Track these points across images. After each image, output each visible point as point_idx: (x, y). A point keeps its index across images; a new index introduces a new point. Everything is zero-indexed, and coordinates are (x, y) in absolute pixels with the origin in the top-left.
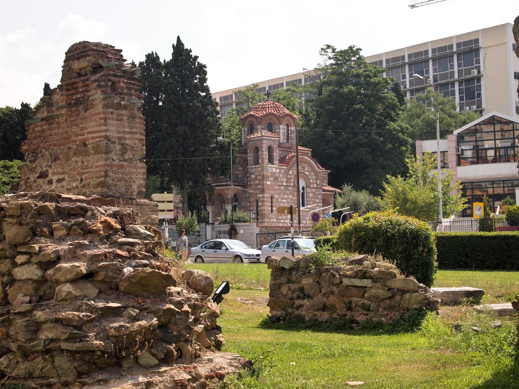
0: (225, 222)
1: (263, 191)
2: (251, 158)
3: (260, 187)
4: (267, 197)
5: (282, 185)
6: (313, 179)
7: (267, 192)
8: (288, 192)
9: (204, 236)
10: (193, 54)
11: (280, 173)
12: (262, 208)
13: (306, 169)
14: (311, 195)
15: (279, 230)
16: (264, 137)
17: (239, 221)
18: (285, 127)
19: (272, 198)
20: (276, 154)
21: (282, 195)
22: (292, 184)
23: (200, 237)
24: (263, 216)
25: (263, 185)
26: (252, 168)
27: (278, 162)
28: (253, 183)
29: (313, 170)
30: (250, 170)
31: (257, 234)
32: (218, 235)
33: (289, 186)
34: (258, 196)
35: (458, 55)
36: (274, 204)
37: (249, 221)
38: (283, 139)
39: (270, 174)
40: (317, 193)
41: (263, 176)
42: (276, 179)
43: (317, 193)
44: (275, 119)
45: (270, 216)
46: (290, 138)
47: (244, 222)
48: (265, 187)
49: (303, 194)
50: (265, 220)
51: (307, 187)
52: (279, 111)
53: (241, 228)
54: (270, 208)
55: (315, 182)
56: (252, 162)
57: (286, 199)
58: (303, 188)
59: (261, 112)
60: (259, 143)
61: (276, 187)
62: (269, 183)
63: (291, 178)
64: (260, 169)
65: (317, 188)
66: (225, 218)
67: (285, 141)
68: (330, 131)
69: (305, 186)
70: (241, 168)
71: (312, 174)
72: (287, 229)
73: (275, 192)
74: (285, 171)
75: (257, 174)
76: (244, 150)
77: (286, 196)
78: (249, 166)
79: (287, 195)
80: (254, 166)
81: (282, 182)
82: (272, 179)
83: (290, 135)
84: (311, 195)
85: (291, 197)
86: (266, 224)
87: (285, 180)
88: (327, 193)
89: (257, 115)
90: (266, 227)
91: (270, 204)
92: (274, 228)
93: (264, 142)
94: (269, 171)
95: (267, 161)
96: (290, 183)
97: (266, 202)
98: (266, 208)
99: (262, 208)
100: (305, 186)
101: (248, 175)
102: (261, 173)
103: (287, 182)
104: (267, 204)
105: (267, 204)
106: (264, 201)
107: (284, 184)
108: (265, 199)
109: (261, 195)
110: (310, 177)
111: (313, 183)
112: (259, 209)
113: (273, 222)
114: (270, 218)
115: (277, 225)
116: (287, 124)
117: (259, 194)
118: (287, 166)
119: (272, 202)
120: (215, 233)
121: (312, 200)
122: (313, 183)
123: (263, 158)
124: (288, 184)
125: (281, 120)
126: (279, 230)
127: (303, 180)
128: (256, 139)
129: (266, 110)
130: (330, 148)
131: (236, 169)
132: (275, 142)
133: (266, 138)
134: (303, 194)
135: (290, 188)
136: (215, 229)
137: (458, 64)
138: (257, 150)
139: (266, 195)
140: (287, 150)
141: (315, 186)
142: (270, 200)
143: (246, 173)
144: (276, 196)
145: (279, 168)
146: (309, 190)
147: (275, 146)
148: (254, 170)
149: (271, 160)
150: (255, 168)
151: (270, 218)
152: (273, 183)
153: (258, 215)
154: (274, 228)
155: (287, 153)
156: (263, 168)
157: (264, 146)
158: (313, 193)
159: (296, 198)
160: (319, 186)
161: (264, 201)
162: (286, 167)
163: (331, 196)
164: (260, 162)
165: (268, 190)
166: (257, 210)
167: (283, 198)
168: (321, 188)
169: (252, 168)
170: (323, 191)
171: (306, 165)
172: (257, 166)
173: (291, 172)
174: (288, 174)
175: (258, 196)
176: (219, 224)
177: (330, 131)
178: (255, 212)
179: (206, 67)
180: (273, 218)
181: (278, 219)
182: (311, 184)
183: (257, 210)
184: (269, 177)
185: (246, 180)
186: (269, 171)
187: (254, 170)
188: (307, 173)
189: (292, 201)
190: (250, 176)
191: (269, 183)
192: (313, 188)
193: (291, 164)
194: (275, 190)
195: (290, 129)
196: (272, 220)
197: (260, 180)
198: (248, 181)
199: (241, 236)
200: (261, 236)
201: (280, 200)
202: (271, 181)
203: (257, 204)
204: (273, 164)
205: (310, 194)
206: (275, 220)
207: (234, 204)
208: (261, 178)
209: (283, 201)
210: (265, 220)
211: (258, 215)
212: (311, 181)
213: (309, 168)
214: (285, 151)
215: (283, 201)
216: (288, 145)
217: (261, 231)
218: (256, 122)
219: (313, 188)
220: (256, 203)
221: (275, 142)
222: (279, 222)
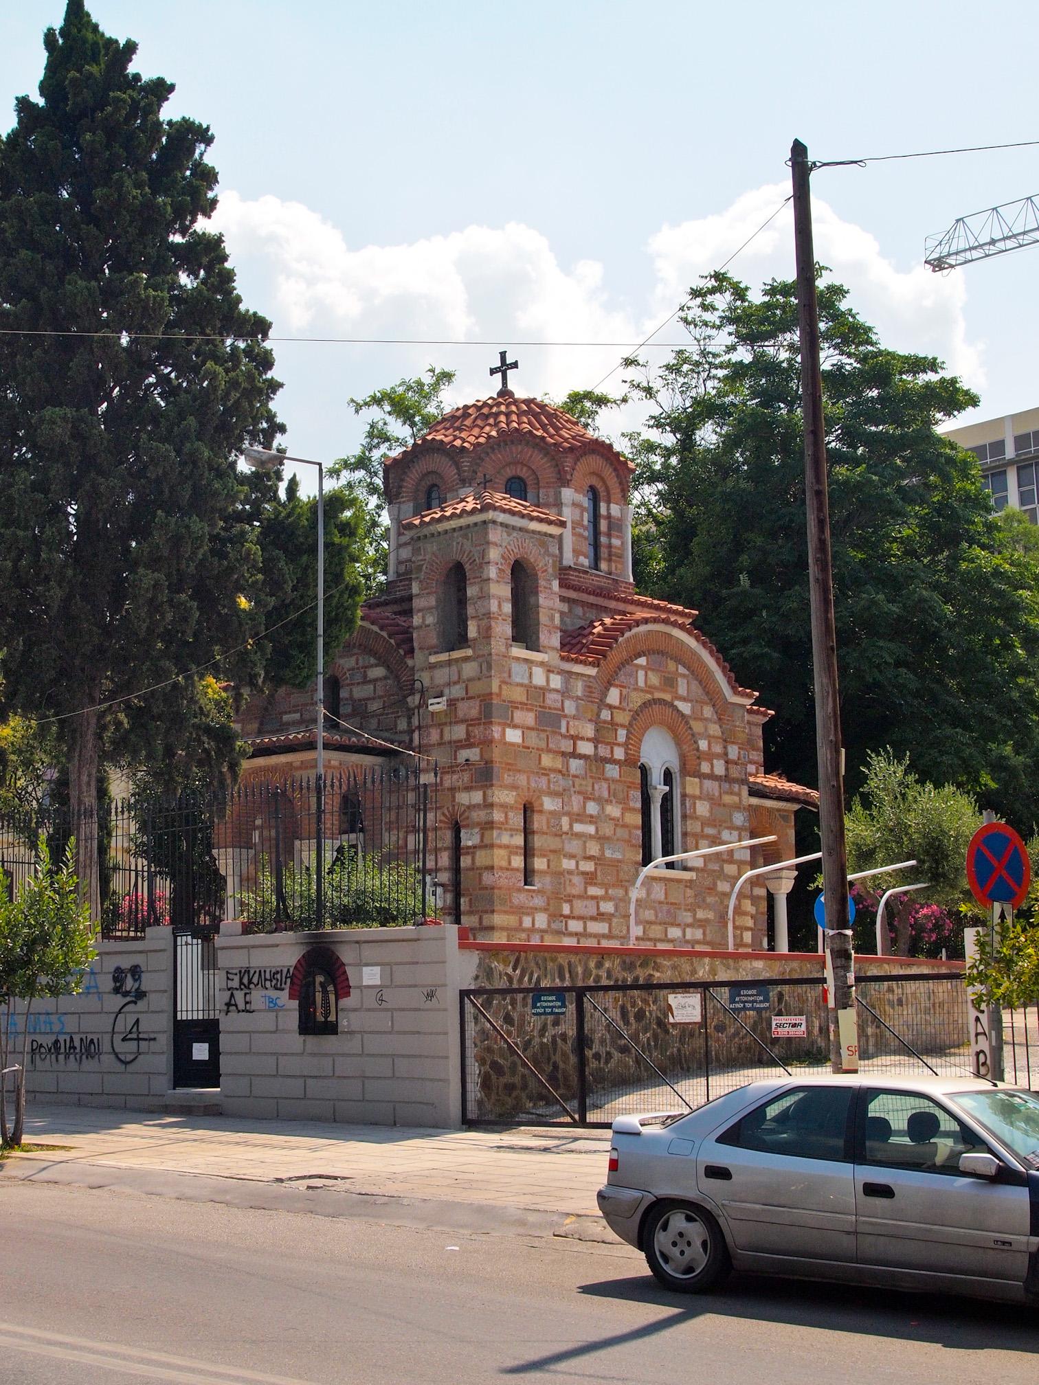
0: (282, 919)
1: (484, 776)
2: (430, 620)
3: (473, 754)
4: (504, 807)
5: (574, 755)
6: (710, 738)
7: (507, 779)
8: (602, 789)
9: (164, 1002)
10: (142, 67)
11: (565, 693)
12: (482, 858)
13: (682, 689)
14: (702, 809)
15: (587, 973)
16: (491, 515)
17: (354, 914)
18: (585, 502)
19: (528, 810)
20: (550, 603)
21: (576, 801)
22: (619, 754)
23: (141, 1005)
24: (487, 901)
25: (487, 742)
26: (432, 667)
27: (555, 640)
28: (434, 736)
29: (712, 696)
30: (425, 678)
31: (464, 994)
32: (239, 997)
33: (606, 760)
34: (463, 798)
35: (1018, 468)
36: (538, 841)
37: (419, 917)
38: (577, 553)
39: (519, 695)
40: (727, 799)
41: (486, 701)
42: (548, 720)
43: (727, 799)
44: (539, 461)
45: (519, 899)
46: (604, 552)
47: (386, 917)
48: (496, 754)
49: (667, 799)
50: (498, 919)
51: (685, 771)
52: (557, 429)
53: (368, 952)
54: (518, 862)
55: (718, 749)
56: (433, 640)
57: (592, 820)
58: (668, 777)
59: (476, 431)
60: (467, 545)
61: (547, 761)
62: (513, 736)
63: (614, 725)
64: (469, 669)
65: (727, 778)
66: (281, 897)
67: (585, 562)
68: (744, 579)
69: (675, 767)
70: (379, 672)
71: (708, 711)
72: (630, 967)
73: (543, 782)
74: (588, 688)
75: (457, 691)
76: (395, 601)
77: (592, 808)
78: (419, 659)
79: (600, 801)
80: (444, 657)
81: (575, 738)
82: (529, 718)
83: (603, 540)
84: (702, 809)
85: (614, 811)
86: (499, 938)
87: (589, 730)
88: (769, 803)
89: (458, 443)
90: (517, 952)
91: (519, 840)
92: (563, 959)
93: (494, 535)
94: (517, 679)
95: (508, 631)
96: (612, 745)
97: (502, 827)
98: (499, 857)
99: (482, 858)
100: (675, 767)
101: (414, 700)
102: (475, 688)
103: (596, 741)
104: (505, 839)
105: (505, 839)
106: (489, 825)
107: (586, 748)
108: (498, 816)
109: (477, 797)
110: (697, 727)
111: (710, 756)
112: (465, 861)
113: (532, 930)
114: (521, 911)
115: (549, 941)
116: (593, 489)
117: (468, 789)
118: (596, 664)
119: (527, 832)
120: (219, 979)
121: (710, 831)
122: (710, 756)
123: (488, 615)
124: (604, 751)
125: (568, 462)
126: (587, 973)
127: (668, 737)
128: (454, 524)
129: (496, 424)
130: (745, 641)
131: (358, 678)
132: (543, 544)
133: (502, 517)
134: (667, 799)
135: (612, 771)
136: (223, 959)
137: (1021, 494)
138: (457, 578)
139: (502, 796)
140: (592, 599)
141: (719, 768)
142: (517, 820)
143: (404, 689)
144: (549, 804)
145: (561, 672)
146: (692, 786)
147: (543, 564)
148: (441, 676)
149: (524, 632)
150: (449, 663)
151: (521, 911)
152: (534, 740)
153: (457, 895)
154: (563, 959)
155: (591, 615)
156: (486, 662)
157: (494, 554)
158: (710, 798)
159: (637, 819)
160: (735, 772)
161: (489, 825)
162: (592, 671)
163: (785, 818)
164: (472, 632)
165: (511, 768)
166: (456, 869)
167: (581, 817)
168: (744, 782)
169: (435, 668)
170: (753, 793)
171: (681, 670)
172: (456, 654)
173: (613, 696)
174: (602, 704)
175: (463, 798)
176: (247, 929)
177: (744, 579)
178: (444, 877)
179: (209, 141)
180: (532, 911)
181: (556, 916)
182: (700, 756)
183: (456, 869)
184: (515, 706)
185: (402, 725)
186: (517, 679)
187: (441, 676)
188: (685, 708)
189: (620, 832)
190: (423, 704)
191: (513, 736)
192: (712, 777)
193: (615, 656)
194: (546, 772)
195: (603, 511)
196: (527, 922)
197: (470, 723)
198: (411, 732)
199: (370, 1001)
200: (488, 1004)
201: (565, 821)
202: (525, 729)
203: (457, 838)
204: (533, 646)
205: (699, 801)
206: (541, 920)
207: (345, 840)
208: (474, 713)
209: (578, 828)
210: (498, 919)
211: (457, 895)
212: (703, 745)
213: (695, 685)
214: (583, 604)
215: (578, 828)
216: (593, 580)
217: (489, 973)
218: (450, 472)
219: (712, 777)
220: (448, 836)
221: (543, 544)
222: (559, 933)
